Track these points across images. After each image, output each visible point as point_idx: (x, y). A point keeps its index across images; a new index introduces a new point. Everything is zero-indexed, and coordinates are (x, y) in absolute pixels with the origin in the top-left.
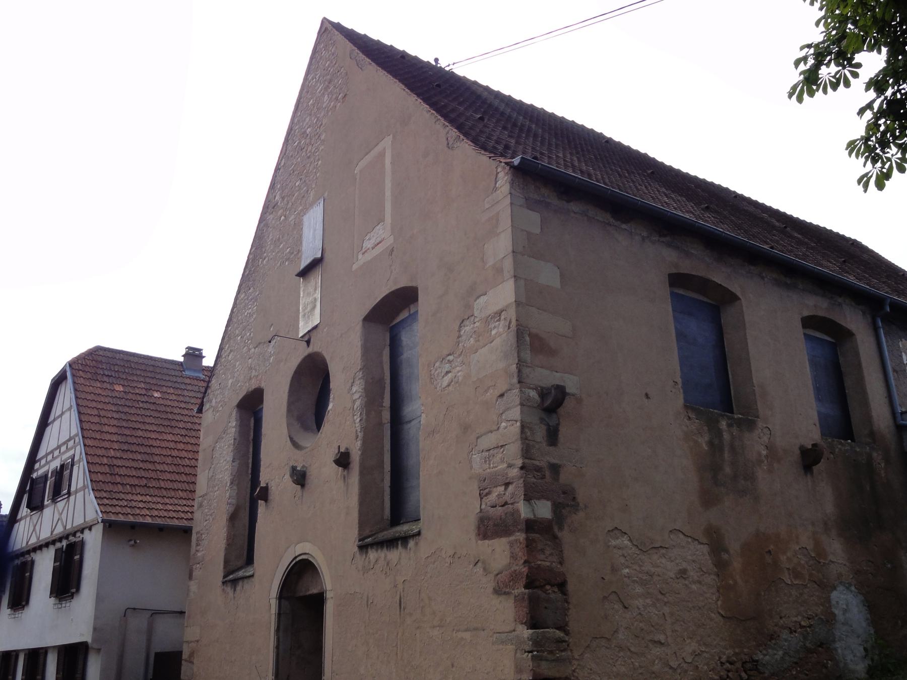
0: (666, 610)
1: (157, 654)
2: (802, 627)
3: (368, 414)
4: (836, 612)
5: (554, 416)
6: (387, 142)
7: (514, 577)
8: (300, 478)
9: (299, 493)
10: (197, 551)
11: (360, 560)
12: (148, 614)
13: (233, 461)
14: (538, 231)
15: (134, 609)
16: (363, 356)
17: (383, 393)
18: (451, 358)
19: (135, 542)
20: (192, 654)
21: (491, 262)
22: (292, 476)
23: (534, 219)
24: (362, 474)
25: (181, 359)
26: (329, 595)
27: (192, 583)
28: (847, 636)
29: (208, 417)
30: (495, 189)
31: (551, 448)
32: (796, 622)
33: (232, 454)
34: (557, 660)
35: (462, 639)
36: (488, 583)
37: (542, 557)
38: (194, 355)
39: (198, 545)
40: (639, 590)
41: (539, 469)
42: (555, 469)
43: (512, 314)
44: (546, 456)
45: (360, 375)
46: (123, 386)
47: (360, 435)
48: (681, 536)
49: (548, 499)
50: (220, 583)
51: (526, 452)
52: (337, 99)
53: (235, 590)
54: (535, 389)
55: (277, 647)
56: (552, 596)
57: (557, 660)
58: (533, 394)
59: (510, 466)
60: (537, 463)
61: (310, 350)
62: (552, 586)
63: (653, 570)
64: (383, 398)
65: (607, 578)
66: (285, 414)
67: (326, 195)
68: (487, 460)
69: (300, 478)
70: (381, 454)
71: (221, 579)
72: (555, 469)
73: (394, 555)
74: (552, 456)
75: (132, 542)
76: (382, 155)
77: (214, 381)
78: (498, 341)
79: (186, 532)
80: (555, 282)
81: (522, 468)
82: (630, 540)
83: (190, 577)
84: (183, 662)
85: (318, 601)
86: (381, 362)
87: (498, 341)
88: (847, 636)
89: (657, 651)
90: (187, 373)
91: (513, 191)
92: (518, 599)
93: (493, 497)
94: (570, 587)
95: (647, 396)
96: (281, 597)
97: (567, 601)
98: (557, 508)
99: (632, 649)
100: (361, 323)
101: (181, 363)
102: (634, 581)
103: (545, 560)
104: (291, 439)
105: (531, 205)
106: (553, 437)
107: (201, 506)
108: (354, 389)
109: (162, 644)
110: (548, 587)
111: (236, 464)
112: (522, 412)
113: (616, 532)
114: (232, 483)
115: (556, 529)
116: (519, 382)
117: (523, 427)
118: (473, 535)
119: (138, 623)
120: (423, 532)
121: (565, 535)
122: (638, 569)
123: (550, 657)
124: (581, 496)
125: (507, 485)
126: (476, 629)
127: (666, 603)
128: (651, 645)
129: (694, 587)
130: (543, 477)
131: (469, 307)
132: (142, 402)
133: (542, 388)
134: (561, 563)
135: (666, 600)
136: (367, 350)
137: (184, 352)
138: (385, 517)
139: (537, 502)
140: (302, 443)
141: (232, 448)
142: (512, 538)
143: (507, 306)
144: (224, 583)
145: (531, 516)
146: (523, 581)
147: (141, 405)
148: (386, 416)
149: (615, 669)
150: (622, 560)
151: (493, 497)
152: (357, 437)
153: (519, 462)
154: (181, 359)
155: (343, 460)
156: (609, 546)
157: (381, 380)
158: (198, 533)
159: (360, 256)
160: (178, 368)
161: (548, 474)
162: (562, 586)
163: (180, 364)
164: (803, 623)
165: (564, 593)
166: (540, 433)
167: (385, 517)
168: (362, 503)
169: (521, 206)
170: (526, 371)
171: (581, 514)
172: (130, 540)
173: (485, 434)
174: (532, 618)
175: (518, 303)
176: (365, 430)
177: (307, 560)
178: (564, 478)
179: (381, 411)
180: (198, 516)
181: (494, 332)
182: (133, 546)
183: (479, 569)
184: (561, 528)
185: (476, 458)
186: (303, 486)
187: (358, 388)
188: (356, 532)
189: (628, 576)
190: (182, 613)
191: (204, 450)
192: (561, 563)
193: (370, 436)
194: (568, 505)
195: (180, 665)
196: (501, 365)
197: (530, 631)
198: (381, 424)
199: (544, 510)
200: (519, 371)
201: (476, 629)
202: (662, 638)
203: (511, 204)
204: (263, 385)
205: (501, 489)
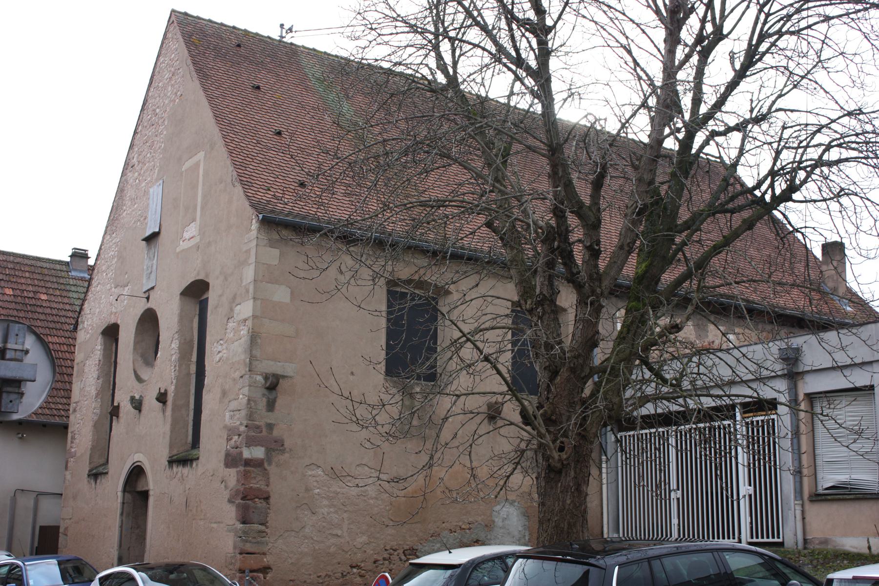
0: (345, 515)
1: (42, 528)
2: (461, 529)
3: (180, 366)
4: (496, 520)
5: (274, 392)
6: (201, 155)
7: (237, 492)
8: (137, 405)
9: (137, 416)
10: (71, 447)
11: (168, 472)
12: (34, 495)
13: (98, 379)
14: (276, 262)
15: (22, 490)
16: (179, 322)
17: (192, 351)
18: (221, 342)
19: (23, 436)
20: (66, 529)
21: (244, 284)
22: (132, 403)
23: (273, 255)
24: (173, 410)
25: (68, 259)
26: (151, 493)
27: (67, 473)
28: (502, 536)
29: (81, 336)
30: (250, 230)
31: (270, 413)
32: (456, 526)
33: (97, 372)
34: (258, 543)
35: (213, 528)
36: (226, 494)
37: (254, 481)
38: (79, 255)
39: (72, 442)
40: (325, 502)
41: (258, 427)
42: (270, 427)
43: (249, 323)
44: (264, 418)
45: (176, 336)
46: (13, 289)
47: (174, 381)
48: (366, 468)
49: (262, 446)
50: (86, 476)
51: (250, 416)
52: (176, 93)
53: (96, 483)
54: (261, 375)
55: (121, 527)
56: (259, 505)
57: (258, 543)
58: (259, 378)
59: (241, 424)
60: (257, 423)
61: (149, 305)
62: (260, 499)
63: (339, 490)
64: (192, 355)
65: (301, 495)
66: (132, 351)
67: (164, 178)
68: (232, 417)
69: (137, 405)
70: (188, 397)
71: (87, 472)
72: (270, 427)
73: (185, 470)
74: (271, 418)
75: (20, 435)
76: (197, 165)
77: (86, 306)
78: (243, 339)
79: (66, 427)
80: (287, 300)
81: (246, 426)
82: (323, 471)
83: (66, 468)
84: (60, 534)
85: (145, 495)
86: (192, 328)
87: (243, 339)
88: (502, 536)
89: (333, 540)
90: (73, 273)
91: (259, 236)
92: (238, 506)
93: (232, 442)
94: (272, 500)
95: (352, 373)
96: (124, 491)
97: (269, 508)
98: (269, 451)
99: (315, 538)
100: (178, 297)
101: (68, 263)
102: (323, 497)
103: (257, 483)
104: (135, 372)
105: (272, 244)
106: (271, 406)
107: (75, 411)
108: (173, 345)
109: (45, 519)
110: (257, 500)
111: (100, 381)
112: (249, 390)
113: (313, 466)
114: (96, 397)
115: (266, 465)
116: (249, 371)
117: (249, 400)
118: (222, 465)
119: (26, 503)
120: (200, 458)
121: (272, 469)
122: (327, 490)
123: (254, 540)
124: (287, 444)
125: (239, 435)
126: (219, 522)
127: (346, 511)
128: (330, 537)
129: (372, 502)
130: (261, 432)
131: (232, 310)
132: (30, 305)
133: (266, 374)
134: (267, 486)
135: (346, 509)
136: (182, 318)
137: (70, 254)
138: (188, 442)
139: (255, 448)
140: (144, 376)
141: (97, 367)
142: (238, 469)
143: (249, 317)
144: (89, 476)
145: (250, 457)
146: (241, 496)
147: (29, 308)
148: (193, 368)
149: (299, 550)
150: (315, 484)
151: (232, 442)
152: (172, 383)
153: (245, 422)
154: (68, 259)
155: (162, 398)
156: (305, 476)
157: (192, 341)
158: (72, 432)
159: (181, 242)
160: (64, 268)
161: (264, 430)
162: (267, 499)
163: (67, 264)
164: (463, 527)
165: (268, 503)
166: (262, 404)
167: (188, 442)
168: (172, 431)
169: (265, 246)
170: (255, 363)
171: (287, 455)
172: (19, 434)
173: (839, 105)
174: (243, 518)
175: (254, 317)
176: (178, 378)
177: (138, 466)
178: (276, 433)
179: (189, 365)
180: (72, 418)
181: (242, 333)
182: (20, 438)
183: (223, 486)
184: (270, 464)
185: (228, 414)
186: (140, 411)
187: (175, 345)
188: (168, 451)
189: (319, 494)
190: (62, 495)
191: (78, 364)
192: (267, 486)
193: (181, 382)
194: (277, 450)
195: (58, 537)
196: (243, 357)
197: (241, 525)
198: (189, 374)
199: (258, 453)
200: (250, 363)
201: (219, 522)
202: (339, 533)
203: (257, 245)
204: (119, 322)
205: (237, 437)
